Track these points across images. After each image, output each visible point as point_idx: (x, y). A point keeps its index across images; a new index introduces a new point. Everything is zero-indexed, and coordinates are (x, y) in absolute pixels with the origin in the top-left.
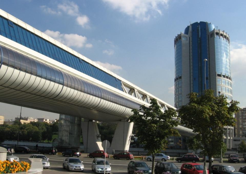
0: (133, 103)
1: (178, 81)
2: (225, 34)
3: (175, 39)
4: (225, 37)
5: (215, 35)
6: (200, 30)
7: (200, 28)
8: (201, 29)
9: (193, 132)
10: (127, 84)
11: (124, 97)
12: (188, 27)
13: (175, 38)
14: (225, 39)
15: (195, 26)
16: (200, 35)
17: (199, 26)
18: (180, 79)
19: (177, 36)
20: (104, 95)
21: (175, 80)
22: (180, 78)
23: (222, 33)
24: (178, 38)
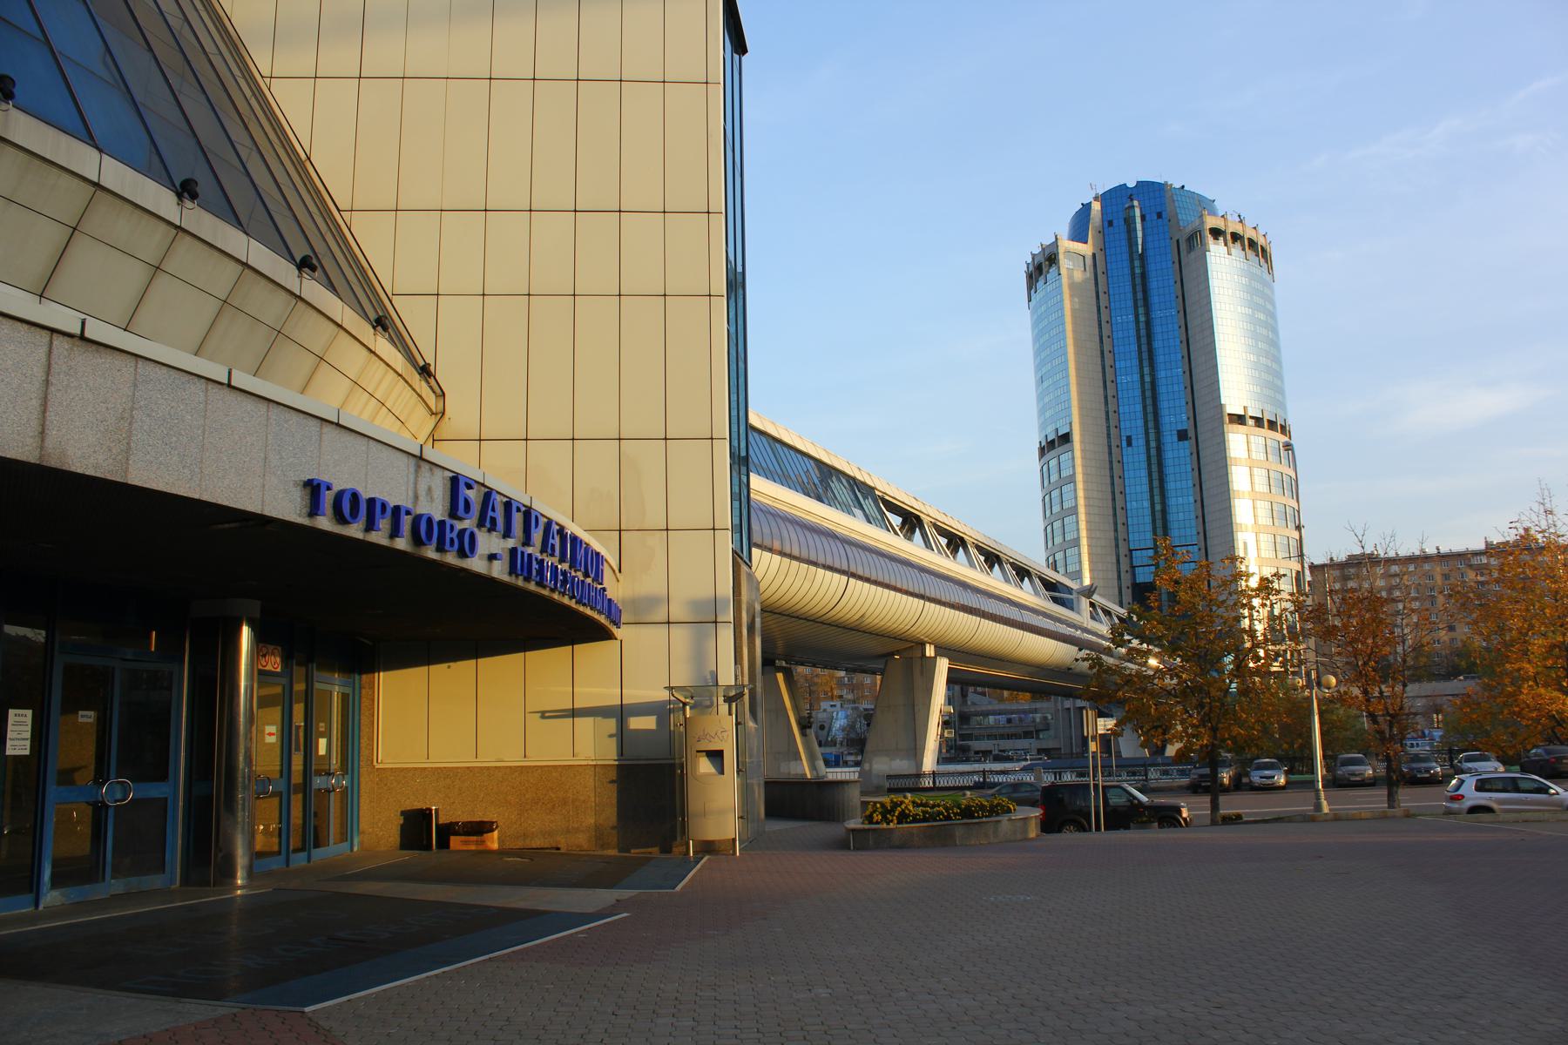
0: (19, 324)
1: (1053, 453)
2: (1249, 234)
3: (1031, 268)
4: (1252, 244)
5: (1210, 239)
6: (1138, 220)
7: (1138, 212)
8: (1143, 218)
9: (407, 855)
10: (989, 549)
11: (839, 530)
12: (1086, 208)
13: (1030, 261)
14: (1250, 253)
15: (1118, 200)
16: (1140, 234)
17: (1136, 203)
18: (1066, 446)
19: (1037, 251)
20: (861, 564)
21: (1043, 451)
22: (1066, 438)
23: (1238, 229)
24: (1043, 260)
